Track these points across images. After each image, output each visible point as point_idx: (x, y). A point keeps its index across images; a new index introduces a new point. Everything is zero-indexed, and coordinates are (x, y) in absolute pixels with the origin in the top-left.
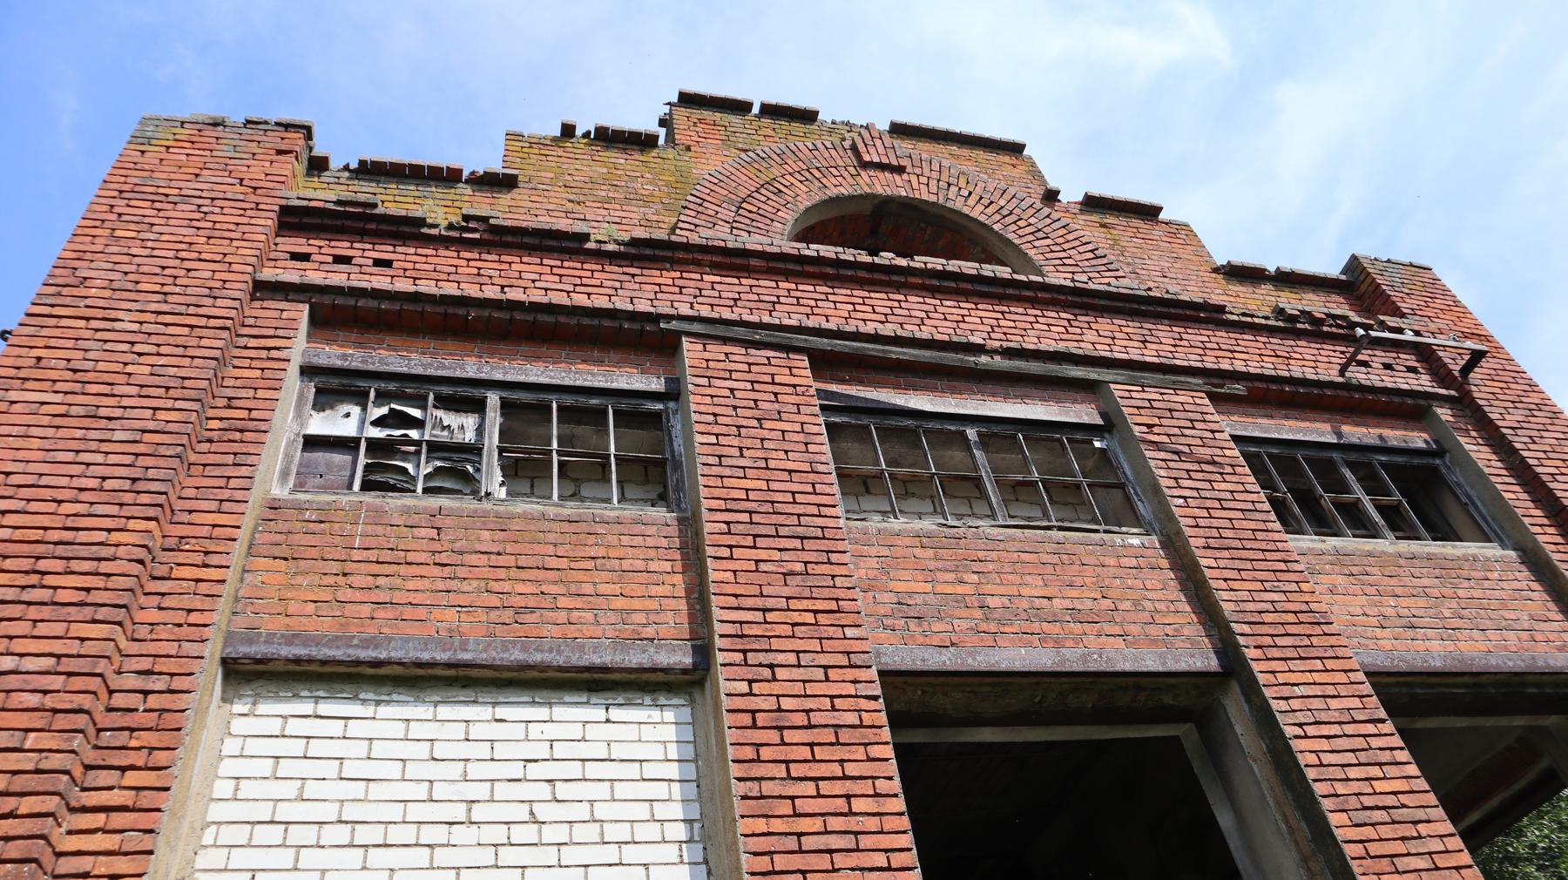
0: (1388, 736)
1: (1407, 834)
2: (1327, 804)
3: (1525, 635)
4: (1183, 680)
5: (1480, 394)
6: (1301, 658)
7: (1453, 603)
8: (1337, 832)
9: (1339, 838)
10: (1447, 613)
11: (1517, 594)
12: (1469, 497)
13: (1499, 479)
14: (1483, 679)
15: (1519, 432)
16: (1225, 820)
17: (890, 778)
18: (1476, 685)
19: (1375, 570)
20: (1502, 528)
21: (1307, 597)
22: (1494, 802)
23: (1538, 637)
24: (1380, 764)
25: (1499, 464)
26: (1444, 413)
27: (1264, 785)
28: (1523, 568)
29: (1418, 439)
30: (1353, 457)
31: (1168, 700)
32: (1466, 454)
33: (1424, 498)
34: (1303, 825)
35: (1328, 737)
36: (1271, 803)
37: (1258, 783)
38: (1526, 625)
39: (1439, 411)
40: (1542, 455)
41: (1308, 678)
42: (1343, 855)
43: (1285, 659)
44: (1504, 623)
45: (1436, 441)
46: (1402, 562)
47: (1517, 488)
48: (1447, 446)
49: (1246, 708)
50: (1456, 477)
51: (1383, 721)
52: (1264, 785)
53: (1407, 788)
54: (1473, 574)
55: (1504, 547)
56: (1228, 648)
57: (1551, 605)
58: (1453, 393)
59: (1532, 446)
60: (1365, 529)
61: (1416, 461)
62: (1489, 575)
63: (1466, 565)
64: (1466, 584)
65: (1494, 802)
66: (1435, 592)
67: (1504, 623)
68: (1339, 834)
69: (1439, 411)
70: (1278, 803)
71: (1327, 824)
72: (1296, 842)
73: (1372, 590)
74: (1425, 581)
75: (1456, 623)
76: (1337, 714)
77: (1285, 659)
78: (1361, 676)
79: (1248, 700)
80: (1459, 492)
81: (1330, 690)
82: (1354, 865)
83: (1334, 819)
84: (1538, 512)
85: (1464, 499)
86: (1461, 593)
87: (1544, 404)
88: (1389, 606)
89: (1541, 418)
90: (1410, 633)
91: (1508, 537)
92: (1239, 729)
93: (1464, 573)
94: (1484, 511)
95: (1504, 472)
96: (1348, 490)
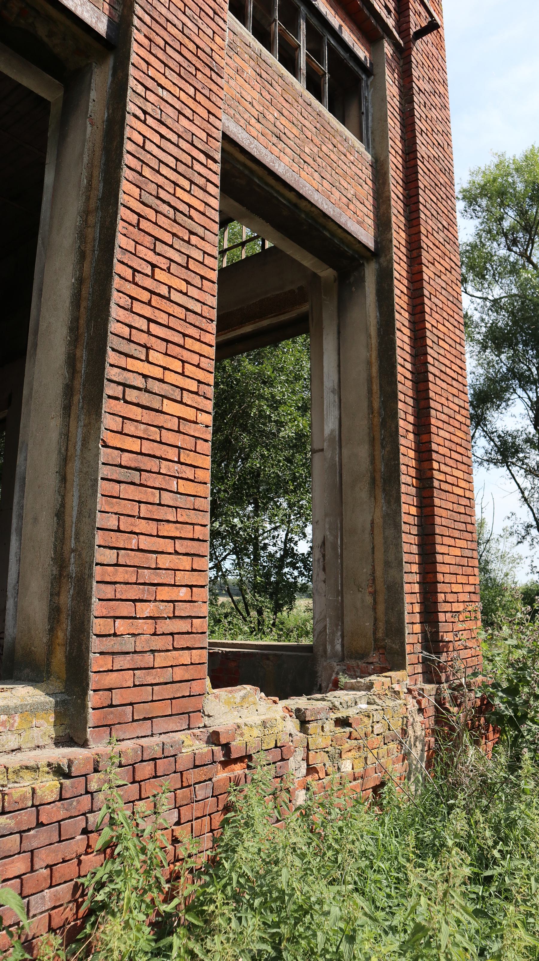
0: (214, 172)
1: (180, 234)
2: (126, 173)
3: (345, 200)
4: (68, 22)
5: (416, 56)
6: (179, 75)
7: (316, 149)
8: (122, 195)
9: (121, 201)
10: (307, 150)
11: (356, 178)
12: (367, 110)
13: (392, 110)
14: (303, 204)
15: (421, 94)
16: (49, 178)
17: (205, 526)
18: (296, 205)
19: (279, 89)
20: (373, 140)
21: (215, 47)
22: (265, 323)
23: (351, 206)
24: (192, 182)
25: (398, 103)
26: (388, 49)
27: (88, 146)
28: (370, 168)
29: (361, 53)
30: (314, 21)
31: (42, 31)
32: (384, 80)
33: (342, 88)
34: (101, 185)
35: (162, 136)
36: (86, 159)
37: (84, 141)
38: (349, 196)
39: (386, 44)
40: (424, 117)
41: (177, 91)
42: (116, 213)
43: (166, 65)
44: (337, 184)
45: (371, 63)
46: (300, 100)
47: (398, 124)
48: (375, 71)
49: (110, 79)
50: (367, 93)
51: (215, 161)
52: (88, 146)
53: (202, 209)
54: (339, 145)
55: (367, 149)
56: (121, 24)
57: (371, 199)
58: (401, 42)
59: (422, 107)
60: (289, 60)
61: (351, 64)
62: (348, 155)
63: (339, 138)
64: (331, 147)
65: (265, 323)
66: (309, 135)
67: (337, 184)
68: (123, 198)
69: (386, 44)
70: (91, 165)
71: (118, 186)
72: (88, 198)
73: (268, 97)
74: (307, 123)
75: (309, 160)
76: (181, 129)
77: (166, 65)
78: (218, 135)
79: (114, 75)
80: (363, 103)
81: (188, 113)
82: (120, 225)
83: (125, 186)
84: (400, 145)
85: (364, 110)
86: (324, 148)
87: (443, 96)
88: (272, 115)
89: (437, 100)
90: (275, 140)
91: (374, 148)
92: (93, 95)
93: (335, 141)
94: (370, 124)
95: (397, 110)
96: (297, 35)
